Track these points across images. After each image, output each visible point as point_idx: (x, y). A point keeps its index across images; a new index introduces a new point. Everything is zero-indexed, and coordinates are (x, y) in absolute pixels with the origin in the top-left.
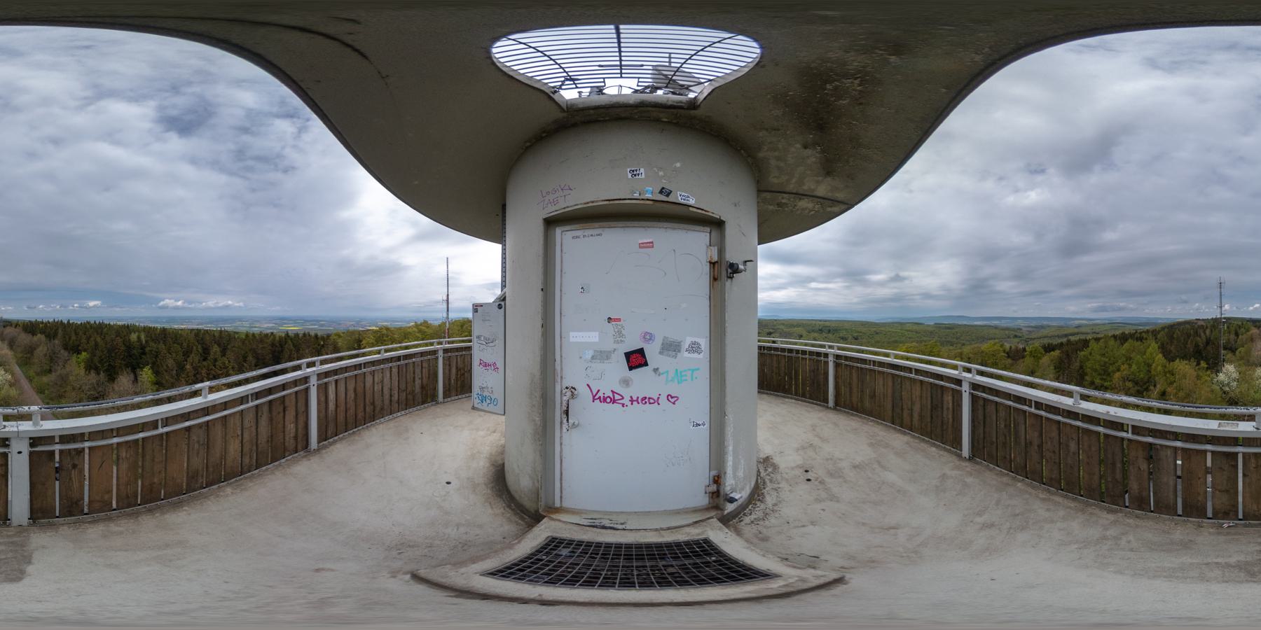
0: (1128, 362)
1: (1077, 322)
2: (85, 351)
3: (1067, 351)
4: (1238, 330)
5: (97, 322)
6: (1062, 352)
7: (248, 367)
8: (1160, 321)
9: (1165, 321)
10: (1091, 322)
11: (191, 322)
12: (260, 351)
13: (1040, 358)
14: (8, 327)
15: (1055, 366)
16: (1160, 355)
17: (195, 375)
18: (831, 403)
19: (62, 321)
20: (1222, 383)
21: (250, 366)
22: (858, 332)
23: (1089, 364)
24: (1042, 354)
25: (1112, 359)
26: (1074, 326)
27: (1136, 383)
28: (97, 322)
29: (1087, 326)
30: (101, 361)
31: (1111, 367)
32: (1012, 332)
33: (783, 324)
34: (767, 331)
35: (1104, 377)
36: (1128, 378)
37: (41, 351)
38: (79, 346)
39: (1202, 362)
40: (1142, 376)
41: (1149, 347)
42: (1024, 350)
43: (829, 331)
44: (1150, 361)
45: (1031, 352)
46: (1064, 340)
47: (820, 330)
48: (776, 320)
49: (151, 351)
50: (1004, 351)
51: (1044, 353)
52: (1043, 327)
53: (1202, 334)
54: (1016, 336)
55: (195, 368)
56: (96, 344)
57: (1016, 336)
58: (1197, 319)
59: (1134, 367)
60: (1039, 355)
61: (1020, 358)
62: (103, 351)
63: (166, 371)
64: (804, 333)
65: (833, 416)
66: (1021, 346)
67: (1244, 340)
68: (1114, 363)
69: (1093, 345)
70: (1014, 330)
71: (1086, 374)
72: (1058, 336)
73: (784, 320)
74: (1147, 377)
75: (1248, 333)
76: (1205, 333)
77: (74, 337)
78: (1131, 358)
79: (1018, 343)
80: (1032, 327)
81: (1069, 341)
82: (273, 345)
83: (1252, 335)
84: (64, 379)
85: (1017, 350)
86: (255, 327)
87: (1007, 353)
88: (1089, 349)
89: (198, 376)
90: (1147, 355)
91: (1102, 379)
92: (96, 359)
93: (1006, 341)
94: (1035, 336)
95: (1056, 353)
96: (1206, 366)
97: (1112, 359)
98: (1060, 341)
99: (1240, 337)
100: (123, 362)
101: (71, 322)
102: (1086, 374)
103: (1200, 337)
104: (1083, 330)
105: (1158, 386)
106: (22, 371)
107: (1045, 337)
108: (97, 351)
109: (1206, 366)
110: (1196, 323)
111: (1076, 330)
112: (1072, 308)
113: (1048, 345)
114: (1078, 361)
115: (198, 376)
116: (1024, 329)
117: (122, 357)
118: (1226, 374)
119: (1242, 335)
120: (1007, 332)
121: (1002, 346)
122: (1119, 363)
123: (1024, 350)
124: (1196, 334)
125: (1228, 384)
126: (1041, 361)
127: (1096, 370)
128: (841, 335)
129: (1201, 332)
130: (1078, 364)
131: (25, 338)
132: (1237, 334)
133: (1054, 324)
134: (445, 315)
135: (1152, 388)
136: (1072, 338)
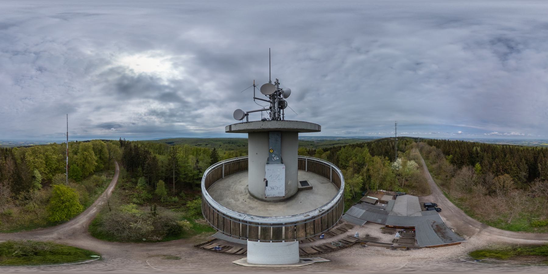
0: (356, 156)
1: (338, 139)
2: (452, 154)
3: (333, 152)
4: (406, 142)
5: (461, 141)
6: (331, 152)
7: (522, 165)
8: (374, 138)
9: (377, 138)
10: (344, 139)
11: (504, 141)
12: (528, 157)
13: (322, 154)
14: (421, 142)
15: (328, 157)
16: (369, 154)
17: (497, 169)
18: (306, 171)
19: (445, 140)
20: (396, 166)
21: (523, 164)
22: (245, 143)
23: (340, 157)
24: (322, 152)
25: (349, 155)
26: (337, 140)
27: (359, 165)
28: (461, 141)
29: (342, 140)
30: (458, 159)
31: (349, 158)
32: (310, 143)
33: (213, 140)
34: (205, 143)
35: (346, 162)
36: (355, 163)
37: (434, 153)
38: (449, 152)
39: (386, 157)
40: (361, 162)
41: (364, 150)
42: (315, 151)
43: (233, 143)
44: (365, 156)
45: (318, 152)
46: (332, 146)
47: (229, 143)
48: (209, 139)
49: (480, 156)
50: (307, 151)
51: (323, 152)
52: (323, 141)
53: (391, 144)
54: (311, 145)
55: (497, 165)
56: (456, 152)
57: (311, 145)
58: (390, 137)
59: (358, 158)
60: (322, 153)
61: (313, 154)
62: (458, 155)
63: (484, 166)
64: (222, 144)
65: (307, 173)
66: (314, 149)
67: (409, 147)
68: (350, 157)
69: (342, 149)
70: (310, 142)
71: (339, 161)
72: (330, 145)
73: (212, 139)
74: (363, 163)
75: (411, 144)
76: (392, 144)
77: (448, 148)
78: (357, 155)
79: (313, 148)
80: (319, 140)
81: (334, 147)
82: (535, 154)
83: (412, 145)
84: (440, 167)
85: (312, 151)
86: (531, 144)
87: (308, 152)
88: (341, 151)
89: (498, 169)
90: (364, 153)
91: (345, 163)
92: (455, 158)
93: (308, 147)
94: (320, 145)
95: (329, 152)
96: (388, 159)
97: (349, 155)
98: (330, 147)
99: (407, 146)
100: (467, 160)
101: (449, 140)
102: (339, 161)
103: (389, 145)
104: (341, 142)
105: (367, 166)
106: (425, 162)
107: (324, 145)
108: (456, 155)
109: (388, 159)
110: (390, 139)
111: (338, 142)
112: (336, 133)
113: (326, 148)
114: (337, 155)
115: (498, 169)
116: (315, 141)
117: (467, 158)
118: (398, 163)
119: (408, 145)
120: (308, 143)
121: (306, 149)
122: (352, 157)
123: (315, 151)
124: (388, 144)
125: (398, 167)
126: (322, 155)
127: (343, 159)
128: (238, 144)
129: (390, 143)
130: (336, 157)
131: (427, 147)
132: (406, 145)
133: (328, 139)
134: (66, 139)
135: (364, 167)
136: (335, 146)
